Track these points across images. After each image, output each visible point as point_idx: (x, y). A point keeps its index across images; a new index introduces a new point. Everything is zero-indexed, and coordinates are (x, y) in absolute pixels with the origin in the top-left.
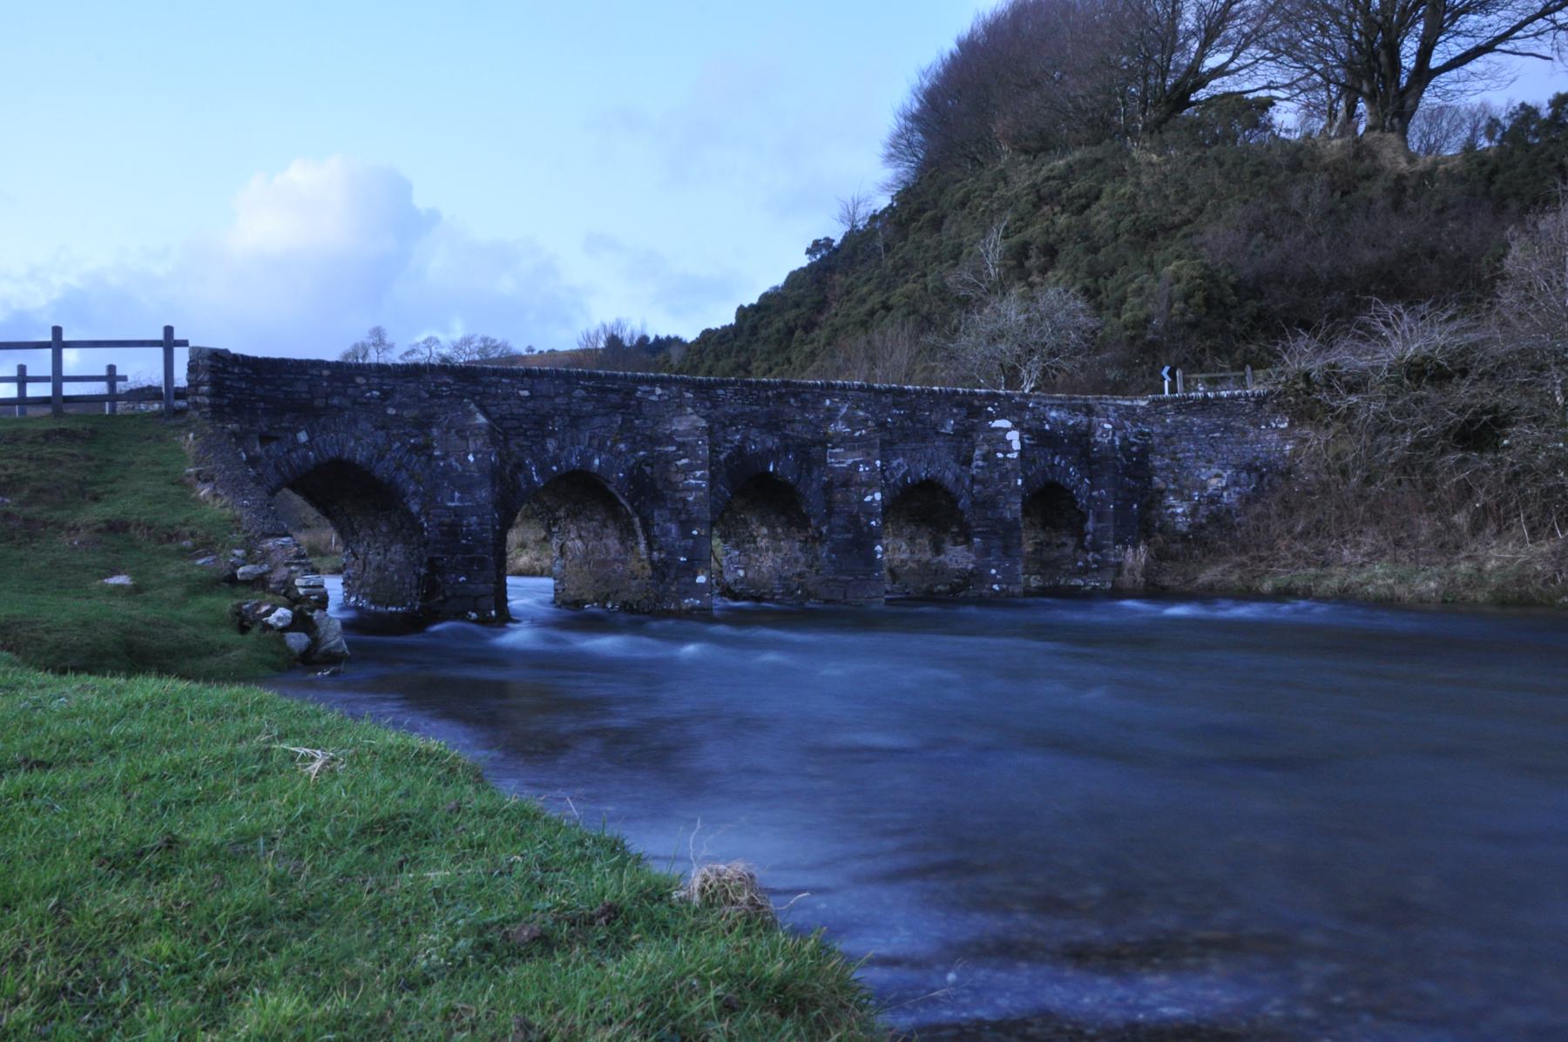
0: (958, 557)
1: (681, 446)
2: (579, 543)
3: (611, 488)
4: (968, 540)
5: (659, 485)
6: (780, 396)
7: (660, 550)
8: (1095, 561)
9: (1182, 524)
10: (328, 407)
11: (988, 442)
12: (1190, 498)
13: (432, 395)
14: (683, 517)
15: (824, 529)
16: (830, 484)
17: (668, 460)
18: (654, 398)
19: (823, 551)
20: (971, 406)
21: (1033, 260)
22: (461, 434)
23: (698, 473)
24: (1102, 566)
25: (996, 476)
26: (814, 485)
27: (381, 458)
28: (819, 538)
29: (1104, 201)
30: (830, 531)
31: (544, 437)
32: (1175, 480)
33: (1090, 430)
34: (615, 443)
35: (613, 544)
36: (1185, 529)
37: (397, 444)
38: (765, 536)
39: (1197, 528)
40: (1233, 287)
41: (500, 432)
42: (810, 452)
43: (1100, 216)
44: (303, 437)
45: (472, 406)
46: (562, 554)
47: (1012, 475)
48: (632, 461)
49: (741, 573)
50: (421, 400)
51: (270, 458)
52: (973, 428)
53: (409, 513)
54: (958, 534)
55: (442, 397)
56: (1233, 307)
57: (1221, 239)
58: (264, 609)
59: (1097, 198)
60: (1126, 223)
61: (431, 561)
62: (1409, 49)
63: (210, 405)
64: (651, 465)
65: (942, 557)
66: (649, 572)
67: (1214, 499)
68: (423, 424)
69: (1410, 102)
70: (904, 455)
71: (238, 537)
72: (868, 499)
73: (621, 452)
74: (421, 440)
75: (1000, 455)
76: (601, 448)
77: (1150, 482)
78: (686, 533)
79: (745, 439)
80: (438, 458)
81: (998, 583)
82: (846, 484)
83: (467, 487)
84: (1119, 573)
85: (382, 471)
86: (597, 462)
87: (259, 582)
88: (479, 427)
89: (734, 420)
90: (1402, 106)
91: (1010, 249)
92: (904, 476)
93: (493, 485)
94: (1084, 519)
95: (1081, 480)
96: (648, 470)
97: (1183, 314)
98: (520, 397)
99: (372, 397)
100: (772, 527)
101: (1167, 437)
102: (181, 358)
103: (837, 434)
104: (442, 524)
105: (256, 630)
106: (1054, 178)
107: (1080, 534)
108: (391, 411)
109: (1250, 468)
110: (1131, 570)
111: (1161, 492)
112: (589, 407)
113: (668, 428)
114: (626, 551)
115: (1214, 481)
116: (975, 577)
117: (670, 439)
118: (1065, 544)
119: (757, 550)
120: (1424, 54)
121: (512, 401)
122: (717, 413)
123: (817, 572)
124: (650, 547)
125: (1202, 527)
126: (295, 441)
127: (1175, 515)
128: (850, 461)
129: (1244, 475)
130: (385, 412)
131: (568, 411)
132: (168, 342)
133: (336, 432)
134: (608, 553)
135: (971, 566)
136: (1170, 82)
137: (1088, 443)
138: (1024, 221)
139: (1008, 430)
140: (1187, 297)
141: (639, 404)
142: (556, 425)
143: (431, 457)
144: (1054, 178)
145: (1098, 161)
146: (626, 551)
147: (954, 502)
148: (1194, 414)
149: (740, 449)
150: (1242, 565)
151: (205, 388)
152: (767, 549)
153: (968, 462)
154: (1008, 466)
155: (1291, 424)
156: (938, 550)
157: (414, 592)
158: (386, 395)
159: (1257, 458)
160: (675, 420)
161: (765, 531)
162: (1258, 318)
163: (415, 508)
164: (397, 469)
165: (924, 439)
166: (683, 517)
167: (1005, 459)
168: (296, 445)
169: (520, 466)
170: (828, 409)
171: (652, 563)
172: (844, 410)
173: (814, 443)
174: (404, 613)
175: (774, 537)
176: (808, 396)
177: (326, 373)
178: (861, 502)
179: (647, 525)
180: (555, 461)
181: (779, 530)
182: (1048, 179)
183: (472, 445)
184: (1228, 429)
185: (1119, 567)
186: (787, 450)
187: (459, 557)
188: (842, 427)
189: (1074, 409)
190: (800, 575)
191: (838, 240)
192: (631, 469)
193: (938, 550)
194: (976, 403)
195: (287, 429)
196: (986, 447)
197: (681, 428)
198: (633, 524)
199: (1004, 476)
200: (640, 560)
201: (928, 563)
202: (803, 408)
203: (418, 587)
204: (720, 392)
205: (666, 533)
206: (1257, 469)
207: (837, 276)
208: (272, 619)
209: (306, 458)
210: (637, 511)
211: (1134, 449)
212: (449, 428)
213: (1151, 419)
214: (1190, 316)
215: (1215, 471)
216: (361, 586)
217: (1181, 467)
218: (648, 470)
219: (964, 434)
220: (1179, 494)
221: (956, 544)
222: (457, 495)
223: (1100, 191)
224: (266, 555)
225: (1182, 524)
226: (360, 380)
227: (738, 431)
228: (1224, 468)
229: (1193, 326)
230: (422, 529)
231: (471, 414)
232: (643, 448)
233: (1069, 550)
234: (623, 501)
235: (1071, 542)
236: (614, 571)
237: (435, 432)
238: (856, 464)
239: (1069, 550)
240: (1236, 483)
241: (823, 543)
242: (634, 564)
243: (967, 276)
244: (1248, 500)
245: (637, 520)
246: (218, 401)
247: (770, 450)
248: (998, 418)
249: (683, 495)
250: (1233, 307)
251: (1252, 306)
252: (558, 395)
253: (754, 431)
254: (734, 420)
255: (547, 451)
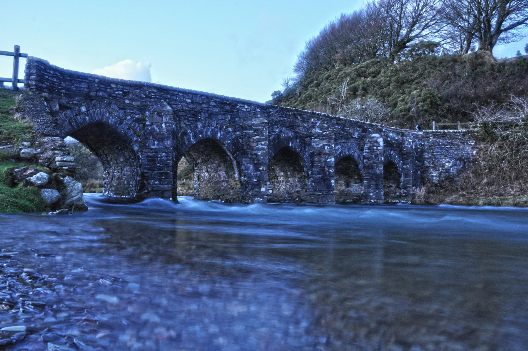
0: (357, 188)
1: (256, 130)
2: (206, 174)
3: (225, 148)
4: (361, 181)
5: (245, 148)
6: (294, 115)
7: (245, 176)
8: (404, 193)
9: (435, 180)
10: (97, 96)
11: (370, 142)
12: (439, 170)
13: (147, 97)
14: (256, 162)
15: (310, 173)
16: (313, 153)
17: (250, 137)
18: (244, 110)
19: (309, 182)
20: (363, 128)
21: (359, 92)
22: (160, 115)
23: (263, 143)
24: (407, 195)
25: (373, 156)
26: (307, 154)
27: (121, 123)
28: (308, 177)
29: (382, 74)
30: (312, 173)
31: (197, 121)
32: (433, 163)
33: (403, 142)
34: (227, 127)
35: (223, 174)
36: (436, 182)
37: (129, 118)
38: (282, 176)
39: (441, 182)
40: (439, 98)
41: (176, 115)
42: (305, 140)
43: (381, 78)
44: (83, 109)
45: (165, 103)
46: (199, 179)
47: (380, 156)
48: (234, 136)
49: (271, 191)
50: (141, 97)
51: (67, 117)
52: (364, 137)
53: (133, 151)
54: (357, 179)
55: (151, 98)
56: (440, 105)
57: (431, 83)
58: (29, 172)
59: (379, 73)
60: (394, 79)
61: (143, 173)
62: (494, 22)
63: (35, 85)
64: (242, 139)
65: (349, 188)
66: (239, 186)
67: (447, 171)
68: (142, 109)
69: (494, 40)
70: (340, 145)
71: (28, 136)
72: (329, 160)
73: (229, 132)
74: (141, 116)
75: (375, 148)
76: (221, 129)
77: (424, 163)
78: (256, 169)
79: (281, 131)
80: (148, 125)
81: (373, 199)
82: (320, 154)
83: (161, 139)
84: (414, 198)
85: (122, 128)
86: (219, 135)
87: (32, 160)
88: (168, 111)
89: (276, 123)
90: (491, 41)
91: (350, 88)
92: (340, 153)
93: (173, 139)
94: (400, 177)
95: (399, 161)
96: (240, 140)
97: (423, 106)
98: (186, 102)
99: (118, 94)
100: (286, 172)
101: (430, 146)
102: (23, 62)
103: (316, 133)
104: (148, 156)
105: (21, 185)
106: (363, 67)
107: (398, 182)
108: (127, 102)
109: (461, 159)
110: (419, 197)
111: (428, 167)
112: (217, 110)
113: (249, 123)
114: (229, 177)
115: (447, 164)
116: (365, 196)
117: (251, 127)
118: (391, 186)
119: (278, 182)
120: (499, 23)
121: (183, 104)
122: (270, 119)
123: (306, 191)
124: (240, 175)
125: (443, 181)
126: (79, 111)
127: (433, 176)
128: (321, 144)
129: (458, 162)
130: (124, 102)
131: (208, 111)
132: (17, 55)
133: (100, 108)
134: (220, 178)
135: (362, 192)
136: (400, 39)
137: (402, 147)
138: (353, 80)
139: (378, 138)
140: (424, 100)
141: (238, 111)
142: (202, 116)
143: (145, 125)
144: (363, 67)
145: (378, 62)
146: (229, 177)
147: (357, 166)
148: (440, 138)
149: (278, 136)
150: (463, 196)
151: (33, 77)
152: (283, 181)
153: (362, 150)
154: (378, 152)
155: (476, 143)
156: (348, 185)
157: (134, 188)
158: (125, 94)
159: (463, 156)
160: (253, 120)
161: (282, 174)
162: (448, 110)
163: (136, 148)
164: (129, 129)
165: (347, 139)
166: (256, 162)
167: (377, 149)
168: (80, 113)
169: (185, 133)
170: (312, 123)
171: (241, 182)
172: (318, 124)
173: (307, 136)
174: (128, 198)
175: (286, 176)
176: (305, 116)
177: (97, 80)
178: (325, 162)
179: (239, 165)
180: (201, 132)
181: (289, 173)
182: (361, 67)
183: (164, 120)
184: (453, 144)
185: (414, 196)
186: (296, 138)
187: (156, 172)
188: (318, 130)
189: (398, 133)
190: (297, 192)
191: (282, 92)
192: (233, 139)
193: (348, 185)
194: (365, 127)
195: (77, 105)
196: (369, 144)
197: (256, 123)
198: (232, 164)
199: (376, 156)
200: (235, 181)
201: (343, 190)
202: (303, 121)
203: (135, 186)
204: (271, 110)
205: (247, 169)
206: (463, 160)
207: (282, 103)
208: (33, 179)
209: (84, 119)
210: (235, 158)
211: (419, 150)
212: (154, 112)
213: (424, 139)
214: (426, 108)
215: (448, 160)
216: (111, 187)
217: (435, 158)
218: (240, 140)
219: (361, 138)
220: (435, 168)
221: (356, 183)
222: (156, 142)
223: (380, 71)
224: (41, 145)
225: (435, 180)
226: (113, 86)
227: (277, 127)
228: (451, 159)
229: (426, 111)
230: (139, 159)
231: (164, 106)
232: (239, 131)
233: (393, 189)
234: (229, 154)
235: (394, 186)
236: (223, 186)
237: (147, 113)
238: (324, 146)
239: (393, 189)
240: (455, 165)
241: (309, 178)
242: (232, 183)
243: (334, 97)
244: (459, 172)
245: (235, 162)
246: (40, 84)
247: (290, 137)
248: (373, 133)
249: (256, 152)
250: (440, 105)
251: (447, 105)
252: (203, 103)
253: (284, 128)
254: (276, 123)
255: (197, 128)
